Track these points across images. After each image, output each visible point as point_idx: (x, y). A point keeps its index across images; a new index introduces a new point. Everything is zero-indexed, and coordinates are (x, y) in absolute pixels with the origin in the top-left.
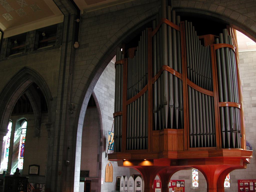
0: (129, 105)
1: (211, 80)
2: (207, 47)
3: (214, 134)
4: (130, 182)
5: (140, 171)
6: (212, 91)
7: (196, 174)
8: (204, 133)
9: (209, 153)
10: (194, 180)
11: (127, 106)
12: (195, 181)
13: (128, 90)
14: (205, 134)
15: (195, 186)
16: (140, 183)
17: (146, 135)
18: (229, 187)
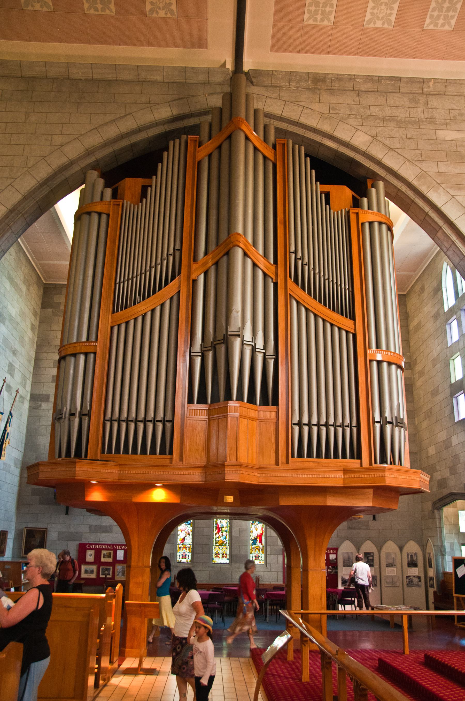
0: (119, 326)
1: (347, 291)
2: (340, 212)
3: (168, 421)
4: (388, 555)
5: (265, 521)
6: (353, 317)
7: (186, 531)
8: (338, 424)
9: (344, 475)
10: (181, 545)
11: (112, 328)
12: (184, 549)
13: (117, 286)
14: (107, 420)
15: (184, 560)
16: (371, 558)
17: (130, 416)
18: (262, 562)
